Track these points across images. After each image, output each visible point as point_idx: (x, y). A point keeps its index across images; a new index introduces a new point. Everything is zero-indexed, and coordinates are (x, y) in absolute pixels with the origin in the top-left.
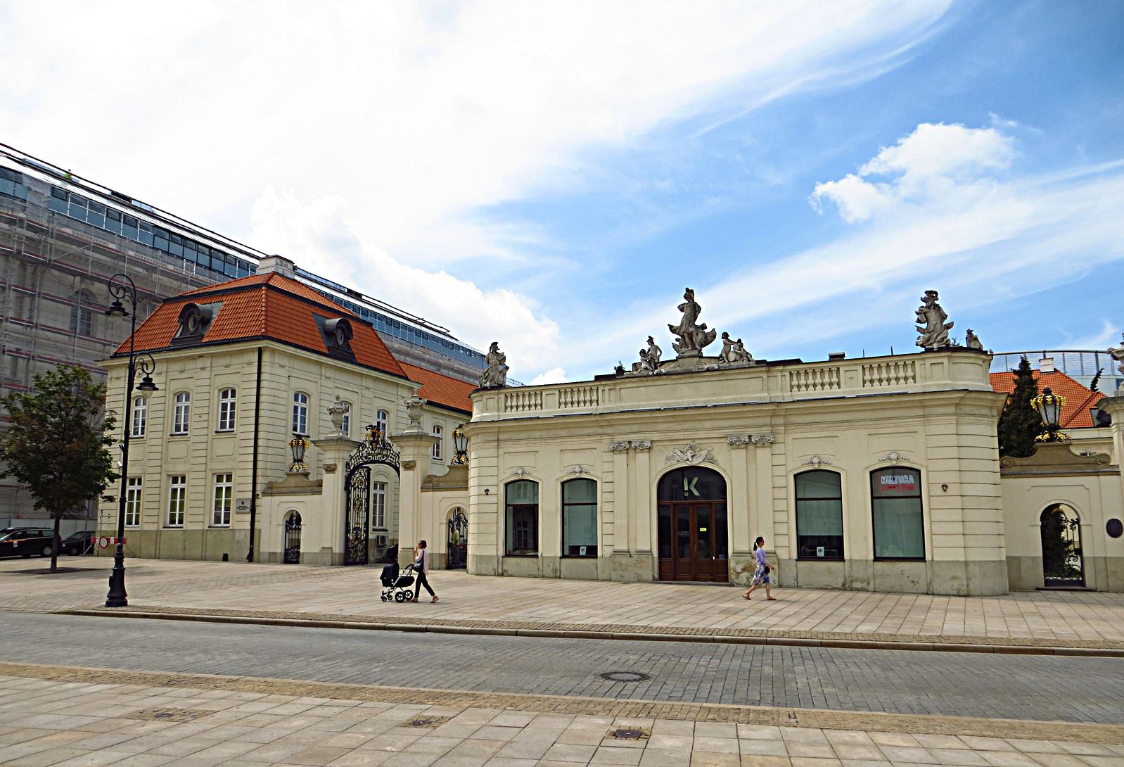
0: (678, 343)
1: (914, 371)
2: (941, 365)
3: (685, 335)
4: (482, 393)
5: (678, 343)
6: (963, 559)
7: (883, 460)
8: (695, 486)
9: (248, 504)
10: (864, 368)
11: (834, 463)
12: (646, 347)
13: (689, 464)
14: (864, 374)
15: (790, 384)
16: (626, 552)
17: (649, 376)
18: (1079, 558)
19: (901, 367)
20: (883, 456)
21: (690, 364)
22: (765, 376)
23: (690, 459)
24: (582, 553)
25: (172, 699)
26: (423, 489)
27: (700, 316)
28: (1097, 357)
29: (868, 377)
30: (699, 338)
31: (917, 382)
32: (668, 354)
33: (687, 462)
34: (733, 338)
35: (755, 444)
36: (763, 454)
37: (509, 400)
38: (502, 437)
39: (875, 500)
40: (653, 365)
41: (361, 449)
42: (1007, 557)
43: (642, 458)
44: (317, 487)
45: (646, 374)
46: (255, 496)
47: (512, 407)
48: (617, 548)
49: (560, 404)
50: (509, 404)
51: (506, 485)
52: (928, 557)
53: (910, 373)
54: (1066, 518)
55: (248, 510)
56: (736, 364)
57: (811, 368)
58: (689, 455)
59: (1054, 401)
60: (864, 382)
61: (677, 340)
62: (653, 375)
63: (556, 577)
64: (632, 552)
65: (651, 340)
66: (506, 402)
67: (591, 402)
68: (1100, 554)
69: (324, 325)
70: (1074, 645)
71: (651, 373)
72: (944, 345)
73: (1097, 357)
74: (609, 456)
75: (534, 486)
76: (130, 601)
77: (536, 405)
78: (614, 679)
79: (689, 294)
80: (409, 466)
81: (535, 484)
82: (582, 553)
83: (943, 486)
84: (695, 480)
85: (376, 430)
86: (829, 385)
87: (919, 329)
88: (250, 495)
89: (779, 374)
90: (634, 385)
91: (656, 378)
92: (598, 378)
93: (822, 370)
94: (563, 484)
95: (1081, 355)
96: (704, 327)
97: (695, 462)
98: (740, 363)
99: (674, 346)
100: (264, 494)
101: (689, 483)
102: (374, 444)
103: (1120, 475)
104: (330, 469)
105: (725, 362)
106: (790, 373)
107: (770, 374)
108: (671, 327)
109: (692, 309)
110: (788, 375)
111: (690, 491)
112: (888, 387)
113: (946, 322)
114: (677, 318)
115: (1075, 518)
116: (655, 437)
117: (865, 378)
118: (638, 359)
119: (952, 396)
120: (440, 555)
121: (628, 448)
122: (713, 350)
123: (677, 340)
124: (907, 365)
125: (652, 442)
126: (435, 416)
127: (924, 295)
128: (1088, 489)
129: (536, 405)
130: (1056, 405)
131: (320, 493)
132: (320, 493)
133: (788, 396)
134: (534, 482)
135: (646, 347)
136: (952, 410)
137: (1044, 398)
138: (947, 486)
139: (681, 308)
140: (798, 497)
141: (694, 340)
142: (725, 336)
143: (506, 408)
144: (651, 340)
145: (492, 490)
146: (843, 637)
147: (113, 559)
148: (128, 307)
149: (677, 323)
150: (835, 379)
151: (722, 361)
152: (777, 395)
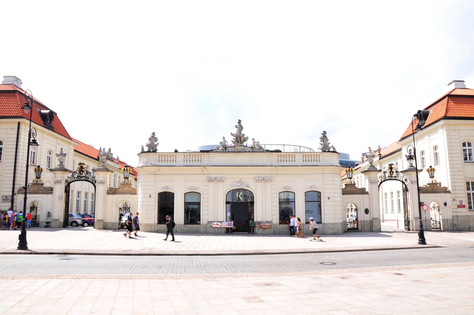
0: (234, 140)
1: (295, 158)
5: (234, 140)
8: (241, 196)
9: (10, 198)
11: (293, 189)
12: (222, 140)
23: (240, 186)
24: (420, 220)
26: (108, 193)
27: (243, 130)
28: (300, 148)
33: (239, 187)
34: (256, 140)
36: (268, 185)
39: (294, 201)
41: (74, 174)
42: (343, 221)
43: (220, 184)
44: (50, 191)
45: (222, 151)
46: (13, 194)
49: (184, 161)
52: (323, 222)
55: (10, 201)
56: (258, 150)
58: (240, 184)
62: (226, 152)
63: (182, 232)
66: (159, 158)
67: (198, 161)
68: (363, 220)
69: (40, 112)
71: (225, 151)
73: (300, 148)
74: (206, 183)
79: (239, 122)
80: (103, 183)
82: (420, 220)
84: (241, 193)
87: (320, 144)
88: (11, 194)
91: (227, 153)
95: (295, 147)
96: (244, 135)
98: (260, 150)
99: (232, 141)
101: (239, 194)
102: (81, 172)
104: (57, 182)
105: (254, 149)
107: (271, 155)
108: (231, 134)
112: (311, 163)
113: (328, 142)
114: (235, 131)
126: (80, 158)
127: (323, 133)
128: (360, 199)
131: (52, 193)
132: (52, 193)
135: (222, 140)
138: (329, 198)
139: (236, 127)
142: (253, 139)
144: (224, 138)
145: (153, 196)
148: (30, 105)
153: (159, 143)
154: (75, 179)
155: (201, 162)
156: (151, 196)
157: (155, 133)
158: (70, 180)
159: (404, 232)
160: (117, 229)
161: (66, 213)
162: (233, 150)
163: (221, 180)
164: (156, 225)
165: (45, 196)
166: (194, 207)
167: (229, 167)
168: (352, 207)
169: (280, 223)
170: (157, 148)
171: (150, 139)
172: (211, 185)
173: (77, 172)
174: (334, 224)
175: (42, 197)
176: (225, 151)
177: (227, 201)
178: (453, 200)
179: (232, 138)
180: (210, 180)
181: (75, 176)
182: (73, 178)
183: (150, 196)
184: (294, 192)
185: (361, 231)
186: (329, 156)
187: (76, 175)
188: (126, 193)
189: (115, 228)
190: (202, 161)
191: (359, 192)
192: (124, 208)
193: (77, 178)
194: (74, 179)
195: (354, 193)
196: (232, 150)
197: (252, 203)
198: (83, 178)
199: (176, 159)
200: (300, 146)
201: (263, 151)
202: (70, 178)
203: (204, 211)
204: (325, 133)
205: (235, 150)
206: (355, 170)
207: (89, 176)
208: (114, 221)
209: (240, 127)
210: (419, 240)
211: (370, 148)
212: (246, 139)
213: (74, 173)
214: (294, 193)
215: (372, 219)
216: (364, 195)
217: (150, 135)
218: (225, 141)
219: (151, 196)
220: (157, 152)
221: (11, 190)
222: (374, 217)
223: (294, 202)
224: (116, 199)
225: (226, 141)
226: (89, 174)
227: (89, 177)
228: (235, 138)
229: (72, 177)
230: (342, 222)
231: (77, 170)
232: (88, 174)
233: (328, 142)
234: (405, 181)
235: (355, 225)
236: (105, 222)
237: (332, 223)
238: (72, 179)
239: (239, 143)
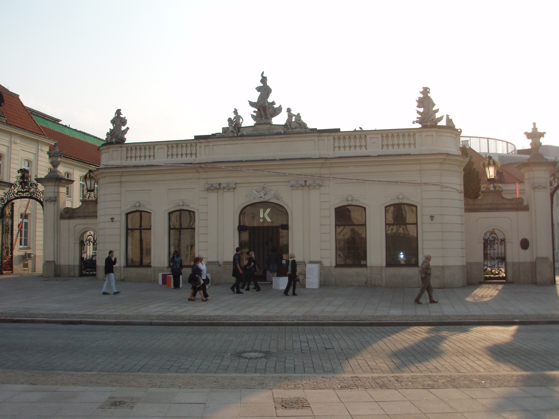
1: (366, 141)
3: (261, 108)
4: (108, 146)
5: (255, 114)
8: (268, 215)
10: (382, 137)
12: (233, 116)
13: (262, 200)
14: (382, 140)
15: (334, 145)
16: (217, 262)
17: (234, 137)
18: (504, 263)
21: (264, 128)
22: (316, 139)
23: (263, 197)
26: (62, 217)
29: (385, 143)
30: (269, 112)
31: (416, 147)
32: (248, 121)
33: (261, 199)
35: (309, 186)
37: (129, 152)
38: (124, 179)
40: (237, 129)
41: (13, 188)
42: (466, 263)
43: (228, 196)
45: (231, 135)
47: (131, 157)
49: (168, 155)
50: (129, 155)
51: (127, 215)
53: (412, 141)
54: (498, 238)
57: (363, 134)
58: (262, 194)
60: (383, 146)
61: (255, 112)
62: (237, 136)
64: (221, 263)
65: (236, 112)
68: (516, 260)
70: (207, 319)
71: (236, 135)
72: (434, 124)
73: (488, 141)
75: (190, 216)
77: (150, 156)
78: (246, 358)
79: (264, 80)
83: (431, 217)
85: (24, 173)
86: (349, 148)
87: (418, 112)
89: (326, 138)
90: (223, 143)
91: (239, 138)
92: (197, 138)
93: (355, 136)
94: (170, 213)
96: (273, 103)
97: (266, 198)
99: (252, 116)
101: (264, 213)
102: (23, 184)
106: (334, 137)
110: (332, 138)
111: (264, 218)
113: (434, 109)
115: (502, 238)
116: (238, 180)
117: (384, 143)
118: (226, 125)
119: (317, 162)
121: (218, 188)
122: (280, 120)
123: (255, 112)
124: (356, 138)
125: (236, 184)
129: (150, 156)
133: (331, 154)
134: (189, 211)
136: (437, 166)
138: (433, 217)
139: (258, 89)
140: (416, 225)
141: (267, 112)
142: (289, 110)
143: (127, 158)
144: (236, 112)
145: (117, 218)
147: (287, 277)
149: (255, 100)
150: (363, 143)
151: (287, 128)
152: (325, 153)
154: (14, 195)
155: (196, 157)
156: (113, 219)
157: (121, 110)
158: (7, 197)
159: (234, 247)
162: (250, 133)
163: (231, 188)
164: (123, 269)
166: (32, 220)
167: (387, 181)
168: (494, 235)
169: (337, 266)
170: (126, 136)
171: (113, 122)
172: (213, 196)
173: (17, 185)
174: (443, 267)
176: (236, 135)
177: (287, 230)
179: (252, 110)
180: (211, 189)
181: (14, 192)
182: (12, 194)
183: (112, 219)
184: (364, 206)
185: (511, 283)
187: (16, 189)
188: (90, 216)
189: (74, 274)
190: (198, 154)
191: (509, 206)
192: (88, 242)
193: (17, 195)
194: (13, 196)
195: (497, 209)
196: (249, 132)
197: (286, 227)
198: (27, 193)
199: (154, 153)
200: (488, 139)
201: (305, 131)
202: (8, 194)
204: (426, 91)
205: (255, 132)
207: (35, 190)
208: (71, 263)
209: (265, 90)
212: (277, 112)
215: (536, 260)
216: (521, 213)
217: (113, 116)
218: (238, 117)
219: (113, 219)
220: (125, 143)
222: (540, 255)
224: (75, 226)
225: (240, 117)
226: (35, 187)
227: (35, 192)
230: (465, 264)
231: (17, 182)
232: (33, 187)
233: (434, 109)
235: (500, 270)
236: (57, 265)
237: (438, 266)
238: (11, 197)
239: (262, 118)
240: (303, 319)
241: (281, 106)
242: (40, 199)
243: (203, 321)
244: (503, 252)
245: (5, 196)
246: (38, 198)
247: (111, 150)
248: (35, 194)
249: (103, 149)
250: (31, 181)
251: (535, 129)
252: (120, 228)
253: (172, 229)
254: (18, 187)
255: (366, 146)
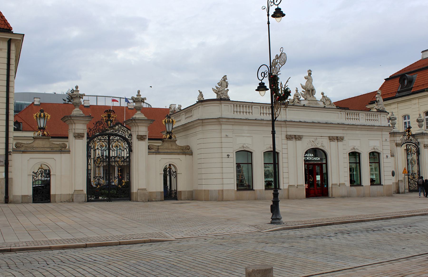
0: (303, 93)
2: (228, 106)
6: (60, 194)
7: (241, 147)
10: (365, 115)
15: (260, 112)
19: (241, 107)
20: (241, 145)
23: (317, 145)
25: (325, 270)
29: (235, 110)
39: (251, 163)
47: (263, 113)
48: (290, 184)
59: (44, 116)
60: (234, 111)
61: (303, 91)
76: (283, 220)
81: (359, 154)
100: (14, 150)
102: (109, 122)
103: (70, 153)
106: (234, 105)
109: (309, 78)
114: (304, 82)
120: (161, 192)
123: (303, 91)
130: (45, 118)
137: (40, 114)
145: (231, 155)
146: (354, 218)
149: (304, 84)
150: (251, 111)
153: (229, 89)
158: (92, 133)
160: (296, 198)
161: (318, 178)
163: (298, 138)
165: (57, 156)
172: (291, 143)
173: (102, 123)
175: (180, 159)
178: (227, 157)
186: (339, 113)
200: (97, 96)
203: (233, 172)
206: (176, 122)
210: (271, 218)
211: (139, 92)
213: (98, 123)
214: (250, 153)
215: (332, 186)
219: (229, 155)
221: (4, 146)
223: (252, 164)
228: (304, 90)
229: (95, 129)
234: (129, 137)
240: (375, 214)
241: (257, 88)
242: (125, 136)
243: (371, 218)
244: (175, 189)
245: (90, 131)
246: (123, 136)
247: (223, 105)
248: (120, 132)
249: (203, 104)
250: (116, 120)
251: (139, 95)
252: (384, 162)
253: (358, 163)
254: (104, 125)
255: (359, 119)
